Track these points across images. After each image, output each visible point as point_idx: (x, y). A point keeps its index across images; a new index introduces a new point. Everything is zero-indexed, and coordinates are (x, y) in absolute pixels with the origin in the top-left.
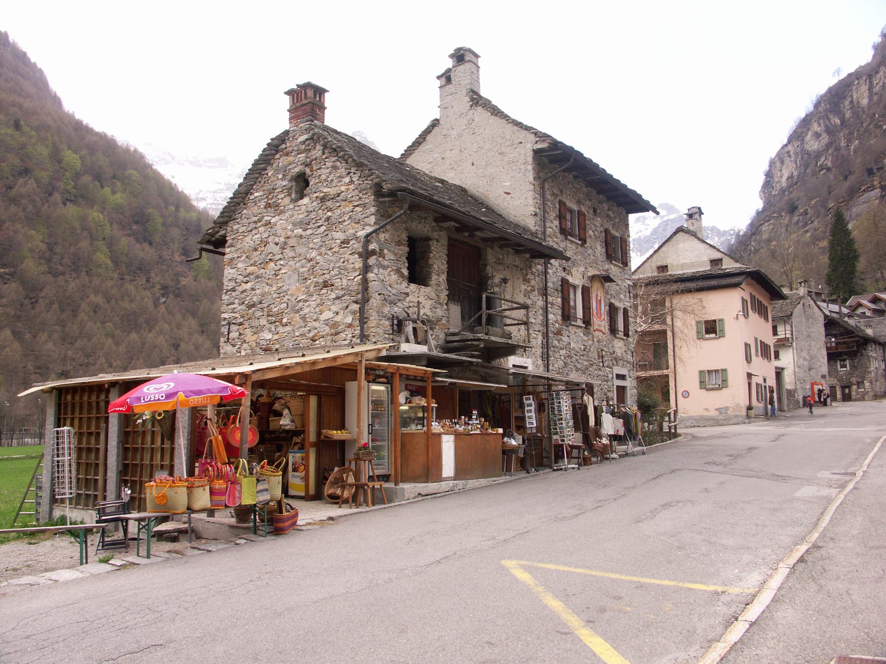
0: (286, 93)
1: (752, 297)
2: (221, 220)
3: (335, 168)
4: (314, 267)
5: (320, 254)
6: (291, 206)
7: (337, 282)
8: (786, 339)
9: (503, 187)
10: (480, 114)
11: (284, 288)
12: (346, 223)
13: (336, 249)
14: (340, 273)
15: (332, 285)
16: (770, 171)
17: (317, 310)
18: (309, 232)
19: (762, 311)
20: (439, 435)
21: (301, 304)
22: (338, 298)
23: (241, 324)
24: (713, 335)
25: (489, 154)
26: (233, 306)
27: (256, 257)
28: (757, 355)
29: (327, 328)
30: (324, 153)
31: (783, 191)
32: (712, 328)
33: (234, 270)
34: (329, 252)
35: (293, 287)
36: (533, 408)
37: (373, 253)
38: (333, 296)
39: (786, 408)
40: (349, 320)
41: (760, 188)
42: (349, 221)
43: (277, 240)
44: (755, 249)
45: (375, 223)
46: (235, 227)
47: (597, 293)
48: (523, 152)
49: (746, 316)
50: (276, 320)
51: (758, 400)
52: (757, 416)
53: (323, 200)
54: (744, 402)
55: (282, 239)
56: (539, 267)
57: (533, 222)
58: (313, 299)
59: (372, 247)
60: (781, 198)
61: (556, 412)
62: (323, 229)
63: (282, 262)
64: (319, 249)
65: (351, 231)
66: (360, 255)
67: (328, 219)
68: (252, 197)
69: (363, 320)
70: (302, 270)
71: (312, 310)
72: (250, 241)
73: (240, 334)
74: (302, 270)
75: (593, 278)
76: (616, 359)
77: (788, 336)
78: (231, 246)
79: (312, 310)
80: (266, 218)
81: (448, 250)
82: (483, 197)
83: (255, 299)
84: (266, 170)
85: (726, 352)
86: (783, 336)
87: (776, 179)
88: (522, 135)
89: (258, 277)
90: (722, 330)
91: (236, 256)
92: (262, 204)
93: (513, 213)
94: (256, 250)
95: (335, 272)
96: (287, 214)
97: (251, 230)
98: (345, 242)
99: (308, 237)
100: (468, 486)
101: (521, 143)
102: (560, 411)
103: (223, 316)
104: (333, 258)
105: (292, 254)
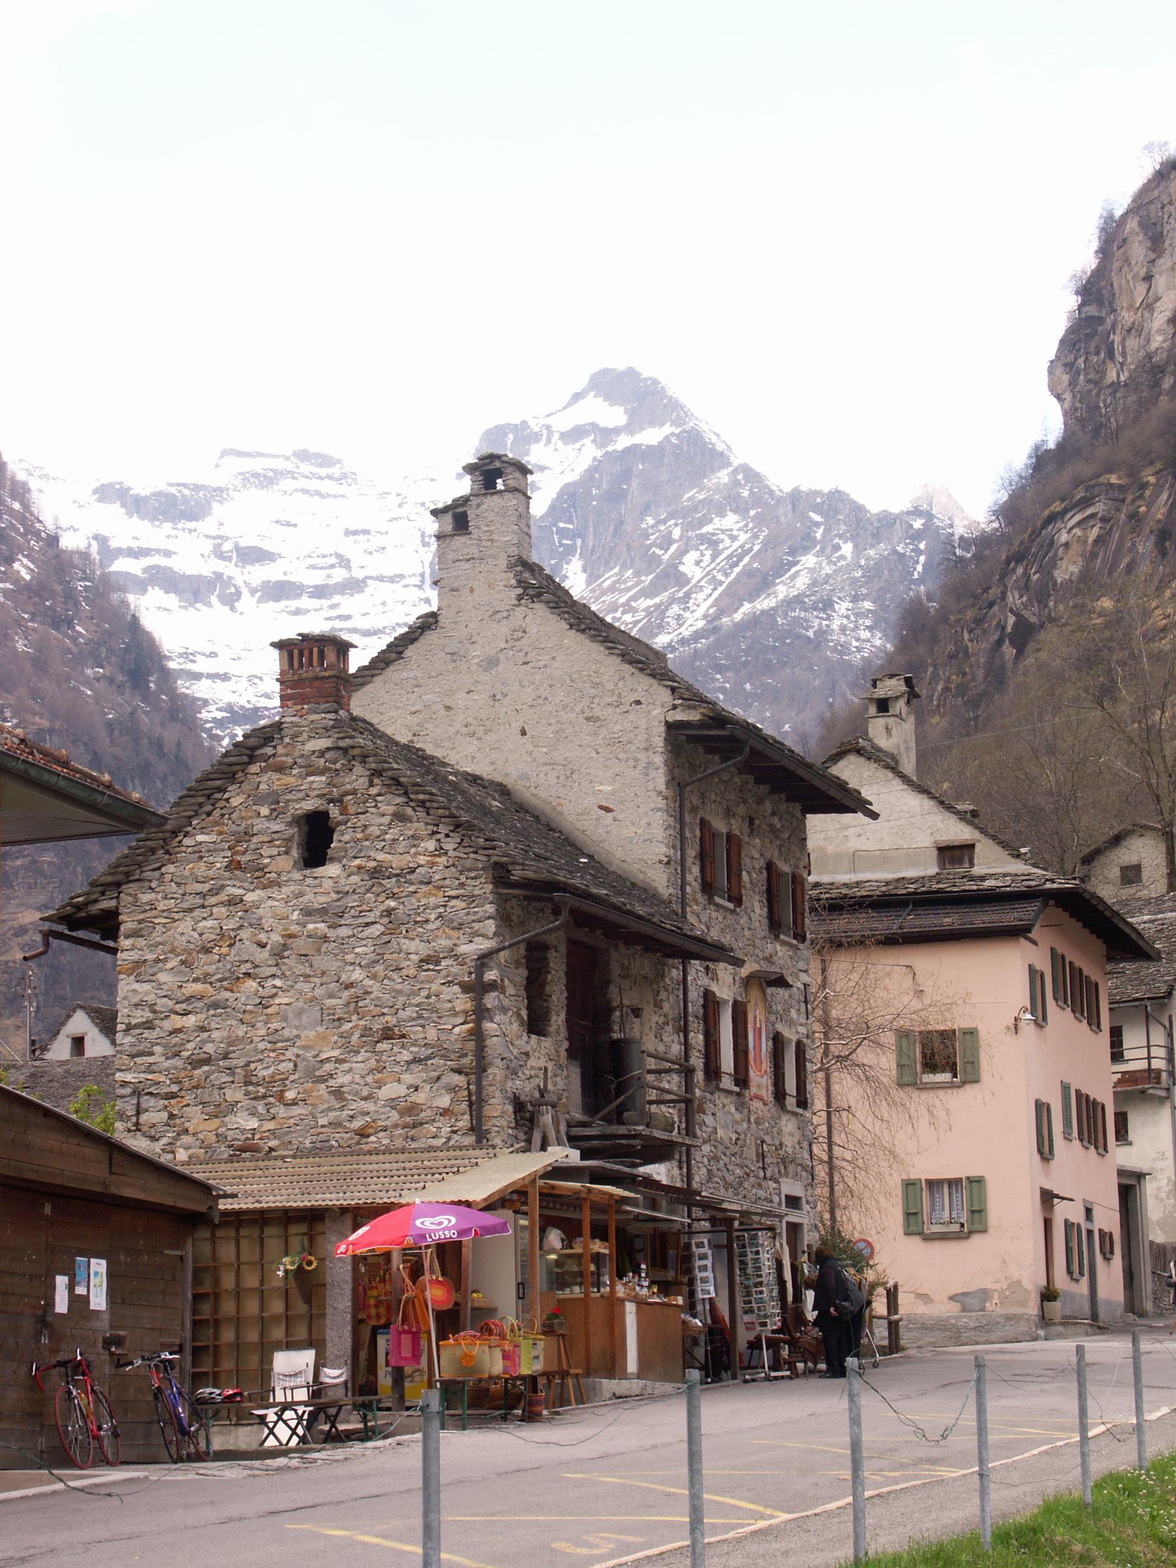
0: (273, 645)
1: (1057, 960)
2: (110, 879)
3: (399, 817)
4: (358, 999)
5: (374, 977)
6: (297, 875)
7: (416, 1032)
8: (1151, 1075)
9: (595, 793)
10: (541, 621)
11: (286, 1033)
12: (430, 926)
13: (412, 972)
14: (420, 1017)
15: (404, 1036)
16: (1099, 275)
17: (369, 1079)
18: (344, 932)
19: (1080, 997)
20: (622, 1301)
21: (328, 1067)
22: (416, 1060)
23: (171, 1096)
24: (945, 1077)
25: (563, 716)
26: (151, 1059)
27: (205, 964)
28: (1067, 1137)
29: (395, 1115)
30: (371, 785)
31: (1153, 370)
32: (941, 1056)
33: (147, 987)
34: (395, 976)
35: (313, 1038)
36: (708, 1263)
37: (492, 986)
38: (406, 1056)
39: (1149, 1306)
40: (445, 1101)
41: (1051, 350)
42: (438, 923)
43: (263, 937)
44: (1021, 622)
45: (495, 934)
46: (146, 897)
47: (756, 1015)
48: (642, 723)
49: (1041, 1021)
50: (270, 1092)
51: (1069, 1272)
52: (1069, 1321)
53: (377, 873)
54: (1032, 1277)
55: (276, 938)
56: (674, 972)
57: (665, 877)
58: (360, 1058)
59: (491, 975)
60: (1145, 405)
61: (750, 1271)
62: (377, 930)
63: (278, 982)
64: (368, 966)
65: (444, 943)
66: (466, 988)
67: (389, 912)
68: (187, 841)
69: (476, 1105)
70: (329, 1002)
71: (358, 1079)
72: (186, 930)
73: (172, 1116)
74: (329, 1002)
75: (748, 982)
76: (785, 1161)
77: (1157, 1064)
78: (136, 934)
79: (358, 1079)
80: (231, 890)
81: (568, 967)
82: (548, 809)
83: (209, 1048)
84: (225, 791)
85: (983, 1130)
86: (1142, 1065)
87: (1127, 317)
88: (643, 686)
89: (215, 1005)
90: (974, 1064)
91: (151, 957)
92: (220, 861)
93: (619, 854)
94: (207, 950)
95: (410, 1012)
96: (285, 890)
97: (191, 910)
98: (431, 960)
99: (342, 942)
100: (656, 1391)
101: (638, 702)
102: (759, 1269)
103: (119, 1076)
104: (406, 987)
105: (301, 969)
